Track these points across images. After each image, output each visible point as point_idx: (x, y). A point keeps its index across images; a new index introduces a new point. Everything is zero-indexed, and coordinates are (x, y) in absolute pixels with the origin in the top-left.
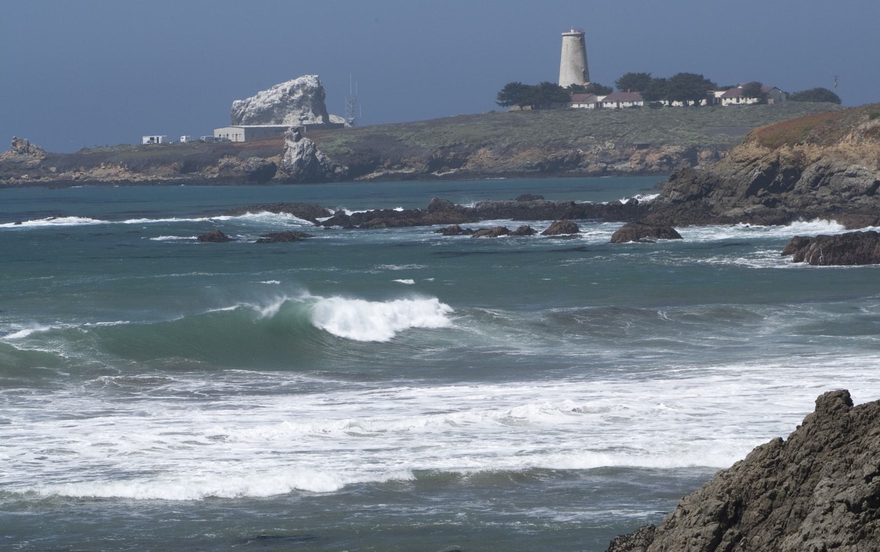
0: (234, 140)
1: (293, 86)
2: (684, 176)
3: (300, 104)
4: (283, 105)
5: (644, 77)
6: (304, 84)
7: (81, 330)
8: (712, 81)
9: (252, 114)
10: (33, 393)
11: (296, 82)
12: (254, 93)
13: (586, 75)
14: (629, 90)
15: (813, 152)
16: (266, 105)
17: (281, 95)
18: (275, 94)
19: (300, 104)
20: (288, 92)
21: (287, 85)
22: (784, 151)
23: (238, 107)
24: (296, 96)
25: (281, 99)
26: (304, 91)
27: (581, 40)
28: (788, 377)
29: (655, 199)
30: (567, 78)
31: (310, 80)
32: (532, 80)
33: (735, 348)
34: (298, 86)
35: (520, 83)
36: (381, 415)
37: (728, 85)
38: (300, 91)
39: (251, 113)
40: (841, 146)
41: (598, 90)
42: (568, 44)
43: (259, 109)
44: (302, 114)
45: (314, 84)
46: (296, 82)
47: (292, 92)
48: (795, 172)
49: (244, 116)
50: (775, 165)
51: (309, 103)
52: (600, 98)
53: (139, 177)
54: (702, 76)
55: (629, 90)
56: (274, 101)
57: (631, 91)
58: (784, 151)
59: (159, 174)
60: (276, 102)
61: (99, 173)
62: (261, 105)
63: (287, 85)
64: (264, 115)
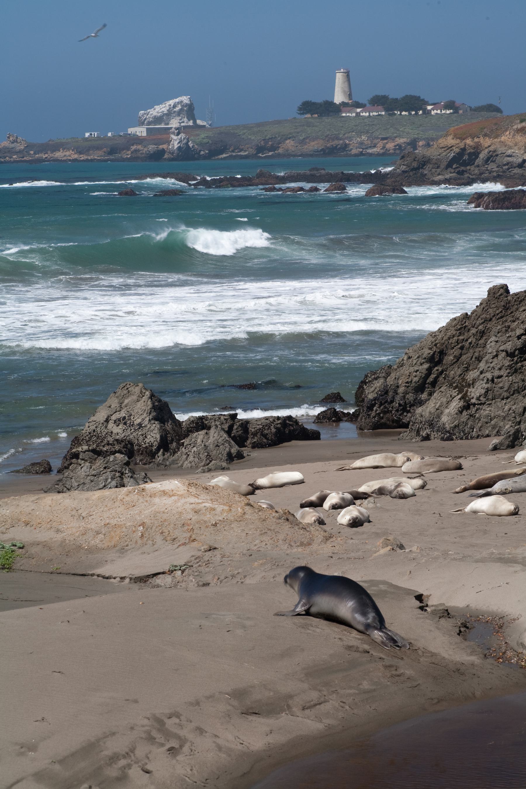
3: (179, 113)
4: (169, 114)
6: (182, 102)
11: (177, 100)
12: (152, 107)
13: (350, 96)
15: (486, 142)
16: (159, 114)
17: (168, 108)
19: (179, 113)
20: (172, 106)
21: (172, 102)
22: (469, 141)
24: (177, 109)
27: (348, 75)
31: (185, 99)
32: (318, 99)
37: (435, 102)
38: (180, 106)
40: (503, 138)
41: (358, 105)
42: (339, 78)
43: (155, 117)
44: (181, 120)
46: (177, 100)
47: (174, 106)
48: (475, 154)
50: (464, 150)
51: (185, 113)
52: (359, 110)
53: (83, 157)
58: (469, 141)
59: (96, 155)
61: (59, 154)
62: (157, 114)
63: (172, 102)
64: (158, 120)
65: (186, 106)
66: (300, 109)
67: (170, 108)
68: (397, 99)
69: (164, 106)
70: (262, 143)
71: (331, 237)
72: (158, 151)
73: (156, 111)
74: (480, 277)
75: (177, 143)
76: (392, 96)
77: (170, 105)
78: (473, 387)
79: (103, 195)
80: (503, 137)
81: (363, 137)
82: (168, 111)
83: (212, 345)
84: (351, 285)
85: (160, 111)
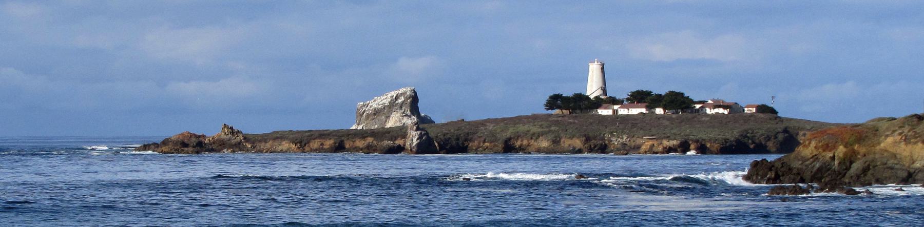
0: (799, 140)
1: (398, 94)
5: (649, 94)
6: (405, 93)
9: (370, 112)
10: (682, 216)
12: (371, 98)
13: (604, 91)
14: (636, 102)
16: (380, 106)
17: (389, 100)
18: (386, 98)
20: (394, 97)
21: (394, 93)
23: (361, 107)
24: (400, 101)
25: (389, 103)
28: (460, 170)
29: (775, 161)
30: (593, 90)
32: (568, 92)
34: (401, 94)
35: (688, 97)
36: (408, 176)
38: (402, 97)
39: (369, 110)
41: (613, 101)
47: (397, 98)
49: (365, 113)
52: (616, 107)
54: (651, 92)
55: (636, 102)
56: (385, 103)
60: (386, 104)
65: (409, 98)
66: (546, 105)
67: (392, 100)
68: (661, 95)
70: (181, 137)
72: (394, 147)
73: (376, 102)
75: (416, 139)
76: (656, 91)
78: (777, 128)
80: (597, 217)
81: (625, 138)
85: (381, 103)
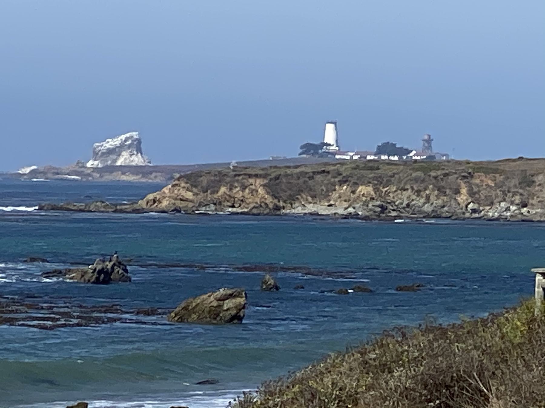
2: (444, 372)
3: (129, 146)
4: (122, 147)
6: (132, 137)
7: (407, 157)
8: (405, 147)
11: (128, 135)
16: (113, 146)
19: (129, 146)
21: (123, 137)
26: (132, 141)
31: (135, 135)
33: (472, 228)
37: (338, 141)
43: (109, 148)
44: (131, 152)
45: (137, 137)
46: (128, 135)
51: (135, 146)
57: (229, 164)
62: (110, 147)
63: (123, 137)
64: (110, 151)
67: (122, 142)
69: (117, 139)
71: (222, 213)
74: (158, 218)
77: (122, 140)
79: (252, 224)
82: (120, 144)
83: (4, 322)
84: (471, 224)
